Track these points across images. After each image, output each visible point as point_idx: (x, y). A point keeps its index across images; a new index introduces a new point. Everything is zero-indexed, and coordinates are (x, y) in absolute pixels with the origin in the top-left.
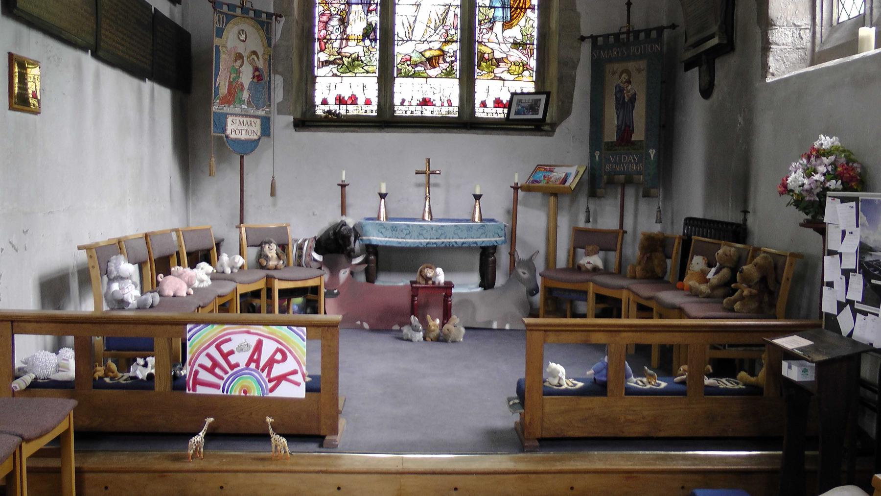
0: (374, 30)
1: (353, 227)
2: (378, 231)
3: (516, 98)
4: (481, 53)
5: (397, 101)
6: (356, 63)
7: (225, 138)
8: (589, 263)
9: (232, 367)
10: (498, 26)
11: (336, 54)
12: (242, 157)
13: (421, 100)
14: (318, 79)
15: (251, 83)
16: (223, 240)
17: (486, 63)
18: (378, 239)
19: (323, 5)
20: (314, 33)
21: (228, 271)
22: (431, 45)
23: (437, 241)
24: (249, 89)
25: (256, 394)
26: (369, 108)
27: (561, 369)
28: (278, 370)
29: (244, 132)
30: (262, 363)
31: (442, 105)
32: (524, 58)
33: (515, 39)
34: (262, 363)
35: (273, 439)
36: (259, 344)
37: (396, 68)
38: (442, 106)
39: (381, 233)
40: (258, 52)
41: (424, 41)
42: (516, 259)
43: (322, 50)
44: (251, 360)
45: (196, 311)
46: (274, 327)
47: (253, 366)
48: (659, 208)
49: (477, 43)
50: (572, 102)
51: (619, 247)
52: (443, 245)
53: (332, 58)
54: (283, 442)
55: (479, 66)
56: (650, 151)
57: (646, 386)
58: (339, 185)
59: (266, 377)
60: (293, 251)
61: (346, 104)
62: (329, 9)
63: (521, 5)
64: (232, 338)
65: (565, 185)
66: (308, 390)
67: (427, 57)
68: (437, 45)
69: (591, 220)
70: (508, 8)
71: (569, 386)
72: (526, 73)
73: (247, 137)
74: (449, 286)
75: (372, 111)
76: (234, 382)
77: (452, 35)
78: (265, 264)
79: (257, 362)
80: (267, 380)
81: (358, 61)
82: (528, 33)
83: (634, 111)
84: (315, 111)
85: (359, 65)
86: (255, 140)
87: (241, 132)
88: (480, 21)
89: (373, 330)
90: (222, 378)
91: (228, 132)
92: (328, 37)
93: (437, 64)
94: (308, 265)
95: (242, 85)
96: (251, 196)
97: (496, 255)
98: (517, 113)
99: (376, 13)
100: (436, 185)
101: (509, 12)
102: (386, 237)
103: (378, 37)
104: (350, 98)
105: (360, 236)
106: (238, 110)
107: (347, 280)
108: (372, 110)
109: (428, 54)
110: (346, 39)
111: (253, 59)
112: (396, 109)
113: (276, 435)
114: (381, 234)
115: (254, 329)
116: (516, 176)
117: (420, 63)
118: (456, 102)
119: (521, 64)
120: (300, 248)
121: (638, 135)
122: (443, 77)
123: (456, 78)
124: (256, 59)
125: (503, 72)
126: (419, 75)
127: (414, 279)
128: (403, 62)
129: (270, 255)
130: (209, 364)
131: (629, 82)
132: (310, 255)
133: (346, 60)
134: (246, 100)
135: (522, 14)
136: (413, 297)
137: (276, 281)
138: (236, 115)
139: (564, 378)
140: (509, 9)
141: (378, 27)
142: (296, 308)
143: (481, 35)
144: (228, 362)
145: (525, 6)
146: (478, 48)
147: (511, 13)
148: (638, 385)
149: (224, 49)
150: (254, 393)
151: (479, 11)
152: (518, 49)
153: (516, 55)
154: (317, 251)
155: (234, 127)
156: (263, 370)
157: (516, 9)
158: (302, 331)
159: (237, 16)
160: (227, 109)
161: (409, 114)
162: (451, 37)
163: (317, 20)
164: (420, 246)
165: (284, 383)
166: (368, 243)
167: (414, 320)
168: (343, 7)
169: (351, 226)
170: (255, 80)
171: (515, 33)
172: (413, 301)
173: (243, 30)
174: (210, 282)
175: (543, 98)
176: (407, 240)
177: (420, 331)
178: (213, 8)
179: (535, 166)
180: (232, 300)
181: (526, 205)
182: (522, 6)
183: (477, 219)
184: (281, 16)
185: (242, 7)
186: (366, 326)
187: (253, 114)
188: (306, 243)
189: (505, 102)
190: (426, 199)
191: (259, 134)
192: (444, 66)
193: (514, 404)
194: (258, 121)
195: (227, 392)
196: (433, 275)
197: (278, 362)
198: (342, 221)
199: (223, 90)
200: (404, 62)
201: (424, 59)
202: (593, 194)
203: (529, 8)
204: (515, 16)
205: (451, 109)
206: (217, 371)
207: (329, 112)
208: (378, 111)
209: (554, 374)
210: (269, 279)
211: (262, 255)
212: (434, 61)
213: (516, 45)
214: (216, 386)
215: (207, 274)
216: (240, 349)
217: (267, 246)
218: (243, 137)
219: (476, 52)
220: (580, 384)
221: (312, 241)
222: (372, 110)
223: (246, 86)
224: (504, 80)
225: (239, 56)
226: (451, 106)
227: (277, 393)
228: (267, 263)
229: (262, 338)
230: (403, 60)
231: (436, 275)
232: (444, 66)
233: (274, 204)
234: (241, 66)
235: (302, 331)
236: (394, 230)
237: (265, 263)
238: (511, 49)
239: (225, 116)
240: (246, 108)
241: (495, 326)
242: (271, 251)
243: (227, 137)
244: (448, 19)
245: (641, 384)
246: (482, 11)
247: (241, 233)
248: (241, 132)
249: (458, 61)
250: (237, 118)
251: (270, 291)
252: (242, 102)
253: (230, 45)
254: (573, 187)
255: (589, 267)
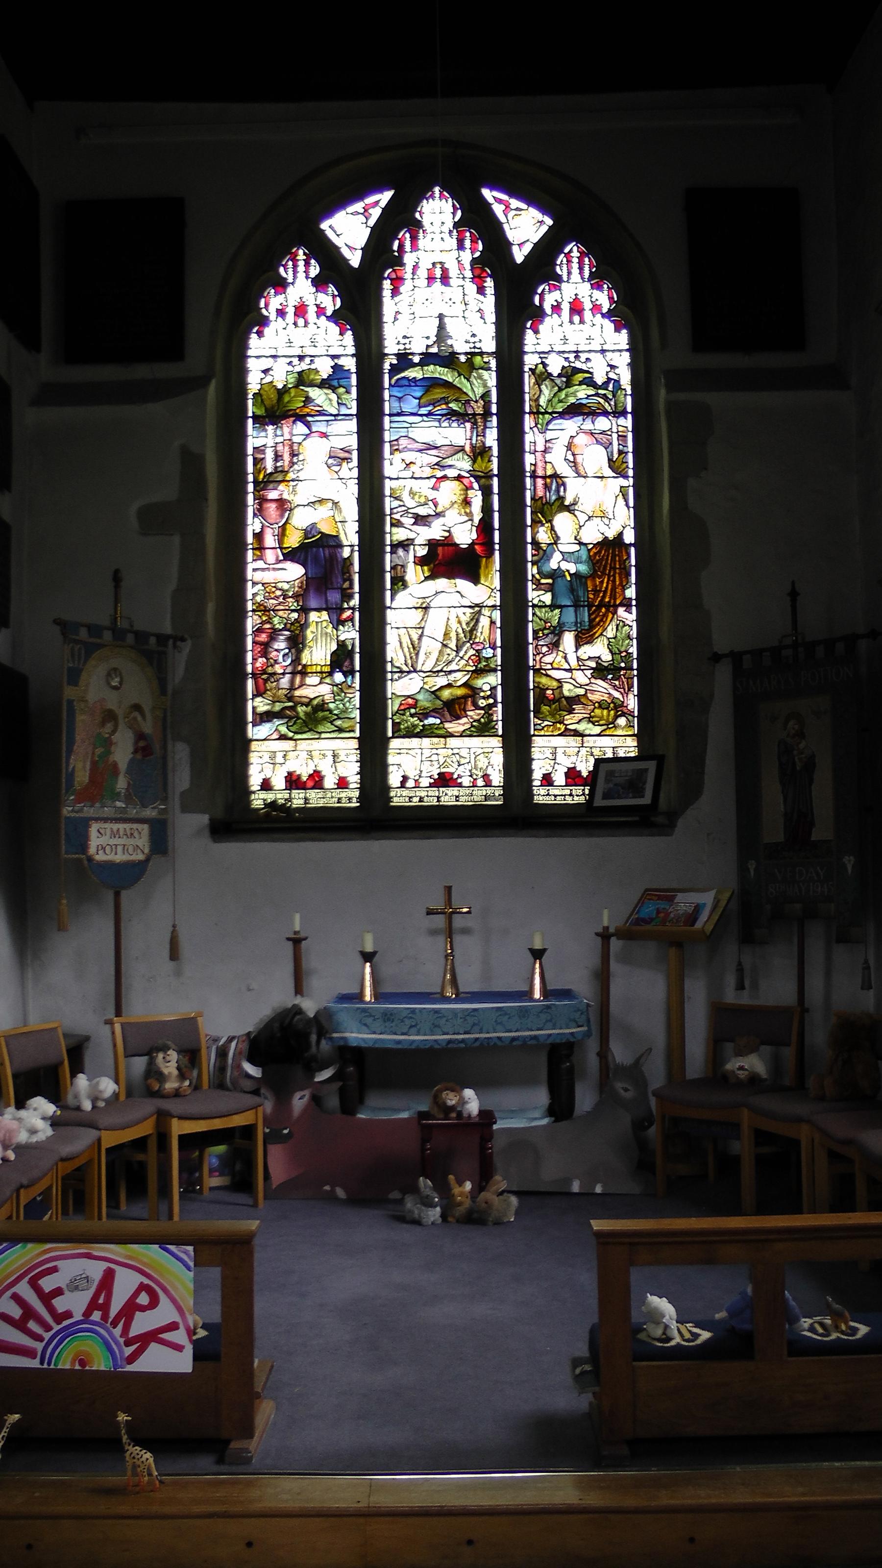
0: (351, 654)
1: (315, 1016)
2: (360, 1022)
3: (603, 767)
4: (540, 688)
5: (394, 780)
6: (321, 714)
7: (86, 862)
8: (741, 1068)
9: (59, 1317)
10: (568, 639)
11: (285, 700)
12: (117, 895)
13: (436, 777)
14: (254, 746)
15: (132, 762)
16: (87, 1039)
17: (550, 706)
18: (361, 1036)
19: (259, 613)
20: (244, 664)
21: (87, 1106)
22: (452, 677)
23: (467, 1036)
24: (129, 771)
25: (103, 1368)
26: (344, 794)
27: (664, 1306)
28: (142, 1323)
29: (120, 849)
30: (114, 1310)
31: (474, 785)
32: (617, 694)
33: (600, 661)
34: (114, 1310)
35: (128, 1453)
36: (108, 1278)
37: (390, 722)
38: (473, 786)
39: (365, 1025)
40: (143, 706)
41: (438, 672)
42: (612, 1066)
43: (258, 693)
44: (93, 1306)
45: (15, 1195)
46: (135, 1247)
47: (96, 1316)
48: (866, 962)
49: (531, 672)
50: (703, 773)
51: (794, 1038)
52: (477, 1044)
53: (278, 707)
54: (147, 1459)
55: (537, 712)
56: (846, 859)
57: (828, 1335)
58: (289, 939)
59: (121, 1337)
60: (209, 1059)
61: (305, 789)
62: (269, 621)
63: (607, 600)
64: (59, 1266)
65: (696, 926)
66: (196, 1358)
67: (445, 700)
68: (461, 678)
69: (747, 983)
70: (585, 606)
71: (684, 1340)
72: (622, 721)
73: (126, 858)
74: (487, 1116)
75: (350, 799)
76: (61, 1347)
77: (487, 659)
78: (157, 1088)
79: (105, 1308)
80: (122, 1340)
81: (323, 710)
82: (623, 649)
83: (813, 787)
84: (249, 802)
85: (325, 719)
86: (140, 862)
87: (114, 850)
88: (535, 632)
89: (357, 1200)
90: (39, 1338)
91: (92, 850)
92: (270, 670)
93: (463, 713)
94: (236, 1087)
95: (115, 765)
96: (137, 958)
97: (493, 1140)
98: (606, 796)
99: (353, 625)
100: (466, 931)
101: (586, 614)
102: (374, 1033)
103: (357, 667)
104: (311, 776)
105: (327, 1032)
106: (107, 811)
107: (305, 1110)
108: (351, 797)
109: (446, 694)
110: (300, 672)
111: (135, 719)
112: (392, 794)
113: (134, 1446)
114: (365, 1028)
115: (99, 1250)
116: (606, 913)
117: (434, 710)
118: (497, 778)
119: (612, 705)
120: (222, 1053)
121: (822, 831)
122: (475, 734)
123: (497, 736)
124: (139, 718)
125: (580, 721)
126: (432, 732)
127: (424, 1108)
128: (401, 711)
129: (166, 1071)
130: (16, 1312)
131: (801, 735)
132: (239, 1067)
133: (301, 709)
134: (123, 791)
135: (610, 616)
136: (424, 1141)
137: (175, 1122)
138: (105, 820)
139: (674, 1325)
140: (586, 608)
141: (357, 650)
142: (215, 1162)
143: (538, 658)
144: (51, 1310)
145: (615, 602)
146: (534, 682)
147: (590, 615)
148: (816, 1333)
149: (82, 705)
150: (99, 1365)
151: (534, 614)
152: (604, 679)
153: (602, 689)
154: (252, 1061)
155: (103, 841)
156: (115, 1324)
157: (599, 607)
158: (186, 1252)
159: (106, 646)
160: (89, 812)
161: (415, 801)
162: (485, 663)
163: (249, 640)
164: (437, 1046)
165: (153, 1346)
166: (342, 1043)
167: (425, 1184)
168: (295, 615)
169: (311, 1014)
170: (139, 756)
171: (599, 649)
172: (423, 1150)
173: (115, 670)
174: (49, 1132)
175: (652, 765)
176: (412, 1038)
177: (435, 1207)
178: (63, 634)
179: (642, 892)
180: (89, 1163)
181: (626, 959)
182: (609, 602)
183: (537, 995)
184: (183, 640)
185: (114, 629)
186: (340, 1193)
187: (136, 816)
188: (233, 1044)
189: (585, 774)
190: (447, 960)
191: (147, 851)
192: (474, 714)
193: (583, 1373)
194: (145, 828)
195: (49, 1364)
196: (458, 1103)
197: (143, 1309)
198: (294, 1005)
199: (82, 777)
200: (404, 710)
201: (439, 703)
202: (747, 938)
203: (621, 605)
204: (598, 620)
205: (489, 791)
206: (32, 1325)
207: (273, 804)
208: (360, 799)
209: (656, 1316)
210: (163, 1118)
211: (153, 1073)
212: (457, 706)
213: (601, 671)
214: (29, 1353)
215: (44, 1118)
216: (74, 1286)
217: (161, 1055)
218: (119, 857)
219: (531, 687)
220: (705, 1335)
221: (244, 1041)
222: (351, 797)
223: (123, 766)
224: (582, 735)
225: (110, 716)
226: (491, 786)
227: (138, 1366)
228: (160, 1087)
229: (112, 1266)
230: (402, 707)
231: (463, 1102)
232: (474, 714)
233: (178, 973)
234: (114, 732)
235: (186, 1252)
236: (389, 1020)
237: (156, 1087)
238: (593, 680)
239: (86, 823)
240: (124, 806)
241: (576, 1187)
242: (168, 1064)
243: (90, 859)
244: (480, 630)
245: (821, 1331)
246: (538, 613)
247: (113, 1033)
248: (114, 850)
249: (500, 706)
250: (108, 825)
251: (163, 1137)
252: (116, 796)
253: (92, 696)
254: (709, 928)
255: (742, 1075)
